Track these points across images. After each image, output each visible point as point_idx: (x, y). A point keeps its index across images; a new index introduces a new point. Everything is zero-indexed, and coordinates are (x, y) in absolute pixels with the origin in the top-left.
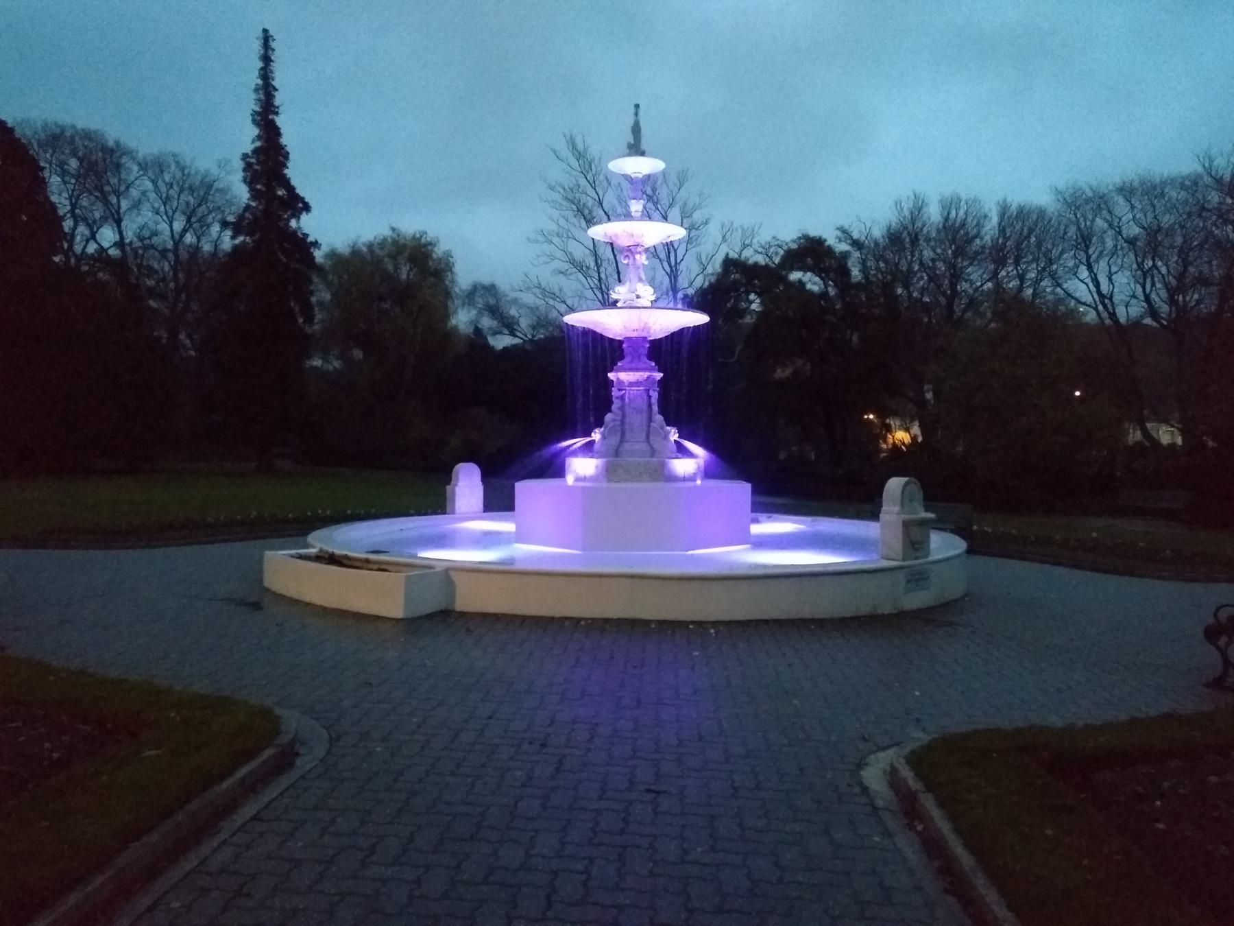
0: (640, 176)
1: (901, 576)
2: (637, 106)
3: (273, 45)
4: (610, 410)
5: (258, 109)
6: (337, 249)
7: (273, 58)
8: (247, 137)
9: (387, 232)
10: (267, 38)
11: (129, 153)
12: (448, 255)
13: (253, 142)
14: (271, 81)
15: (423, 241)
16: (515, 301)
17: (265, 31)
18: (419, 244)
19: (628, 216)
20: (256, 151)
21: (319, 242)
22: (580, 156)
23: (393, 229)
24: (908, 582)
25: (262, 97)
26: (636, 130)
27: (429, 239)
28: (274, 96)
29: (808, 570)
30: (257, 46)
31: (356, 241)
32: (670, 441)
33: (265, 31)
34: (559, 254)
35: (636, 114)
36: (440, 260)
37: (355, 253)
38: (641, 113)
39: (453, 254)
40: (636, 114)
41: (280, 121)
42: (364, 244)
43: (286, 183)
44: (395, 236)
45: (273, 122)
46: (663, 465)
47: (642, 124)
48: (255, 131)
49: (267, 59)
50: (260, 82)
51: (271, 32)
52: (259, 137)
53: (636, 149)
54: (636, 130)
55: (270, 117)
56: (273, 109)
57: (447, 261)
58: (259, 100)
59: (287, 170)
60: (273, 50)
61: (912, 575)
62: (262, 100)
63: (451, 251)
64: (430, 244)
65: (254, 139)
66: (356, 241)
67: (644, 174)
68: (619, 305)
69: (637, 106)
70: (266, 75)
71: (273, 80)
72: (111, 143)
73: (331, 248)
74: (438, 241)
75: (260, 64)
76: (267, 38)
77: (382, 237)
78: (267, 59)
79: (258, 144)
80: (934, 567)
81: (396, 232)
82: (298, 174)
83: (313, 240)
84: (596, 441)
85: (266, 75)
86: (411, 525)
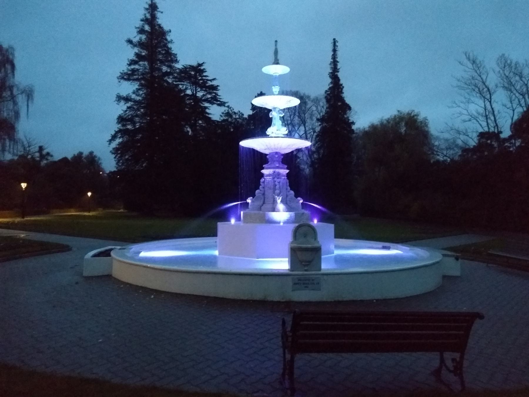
0: (278, 75)
1: (289, 281)
2: (276, 41)
3: (337, 44)
4: (258, 189)
5: (331, 71)
6: (374, 123)
7: (337, 50)
8: (326, 83)
9: (396, 113)
10: (335, 42)
11: (308, 97)
12: (425, 119)
13: (329, 85)
14: (336, 59)
15: (412, 115)
16: (437, 138)
17: (334, 39)
18: (410, 116)
19: (272, 94)
20: (330, 88)
21: (354, 122)
22: (474, 62)
23: (399, 111)
24: (295, 284)
25: (333, 66)
26: (276, 52)
27: (415, 114)
28: (337, 65)
29: (270, 272)
30: (330, 47)
31: (382, 119)
32: (299, 203)
33: (334, 39)
34: (465, 112)
35: (276, 45)
36: (421, 122)
37: (382, 124)
38: (278, 44)
39: (427, 118)
40: (276, 45)
41: (340, 75)
42: (386, 120)
43: (342, 100)
44: (399, 114)
45: (337, 75)
46: (264, 215)
47: (279, 50)
48: (330, 80)
49: (335, 51)
50: (332, 60)
51: (336, 39)
52: (331, 83)
53: (276, 62)
54: (276, 52)
55: (336, 74)
56: (337, 70)
57: (425, 122)
58: (332, 68)
59: (124, 103)
60: (337, 46)
61: (299, 280)
62: (333, 68)
63: (427, 117)
64: (416, 115)
65: (329, 84)
66: (382, 119)
67: (280, 74)
68: (270, 136)
69: (276, 41)
70: (334, 57)
71: (337, 58)
72: (302, 95)
73: (372, 123)
74: (420, 114)
75: (332, 53)
76: (335, 42)
77: (394, 116)
78: (335, 51)
79: (331, 86)
80: (325, 277)
81: (400, 112)
82: (348, 96)
83: (352, 121)
84: (250, 203)
85: (334, 57)
86: (191, 242)
